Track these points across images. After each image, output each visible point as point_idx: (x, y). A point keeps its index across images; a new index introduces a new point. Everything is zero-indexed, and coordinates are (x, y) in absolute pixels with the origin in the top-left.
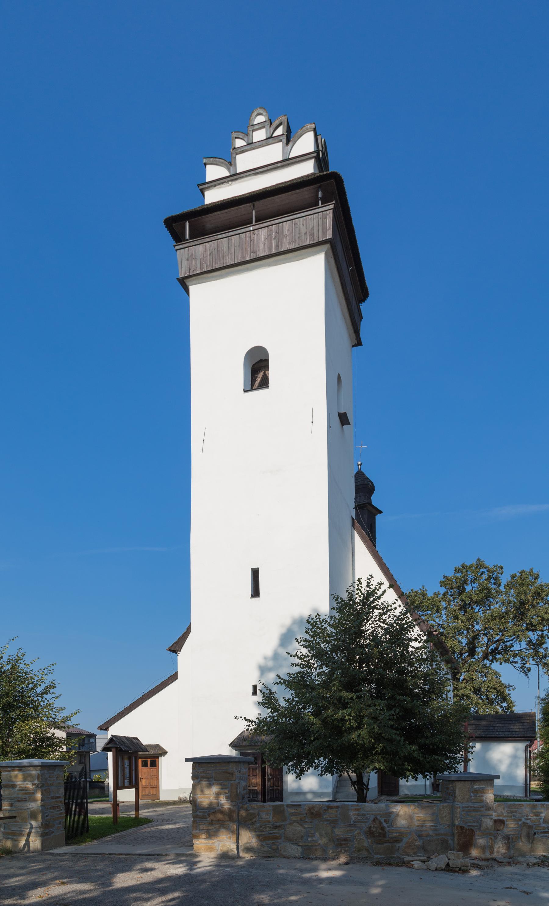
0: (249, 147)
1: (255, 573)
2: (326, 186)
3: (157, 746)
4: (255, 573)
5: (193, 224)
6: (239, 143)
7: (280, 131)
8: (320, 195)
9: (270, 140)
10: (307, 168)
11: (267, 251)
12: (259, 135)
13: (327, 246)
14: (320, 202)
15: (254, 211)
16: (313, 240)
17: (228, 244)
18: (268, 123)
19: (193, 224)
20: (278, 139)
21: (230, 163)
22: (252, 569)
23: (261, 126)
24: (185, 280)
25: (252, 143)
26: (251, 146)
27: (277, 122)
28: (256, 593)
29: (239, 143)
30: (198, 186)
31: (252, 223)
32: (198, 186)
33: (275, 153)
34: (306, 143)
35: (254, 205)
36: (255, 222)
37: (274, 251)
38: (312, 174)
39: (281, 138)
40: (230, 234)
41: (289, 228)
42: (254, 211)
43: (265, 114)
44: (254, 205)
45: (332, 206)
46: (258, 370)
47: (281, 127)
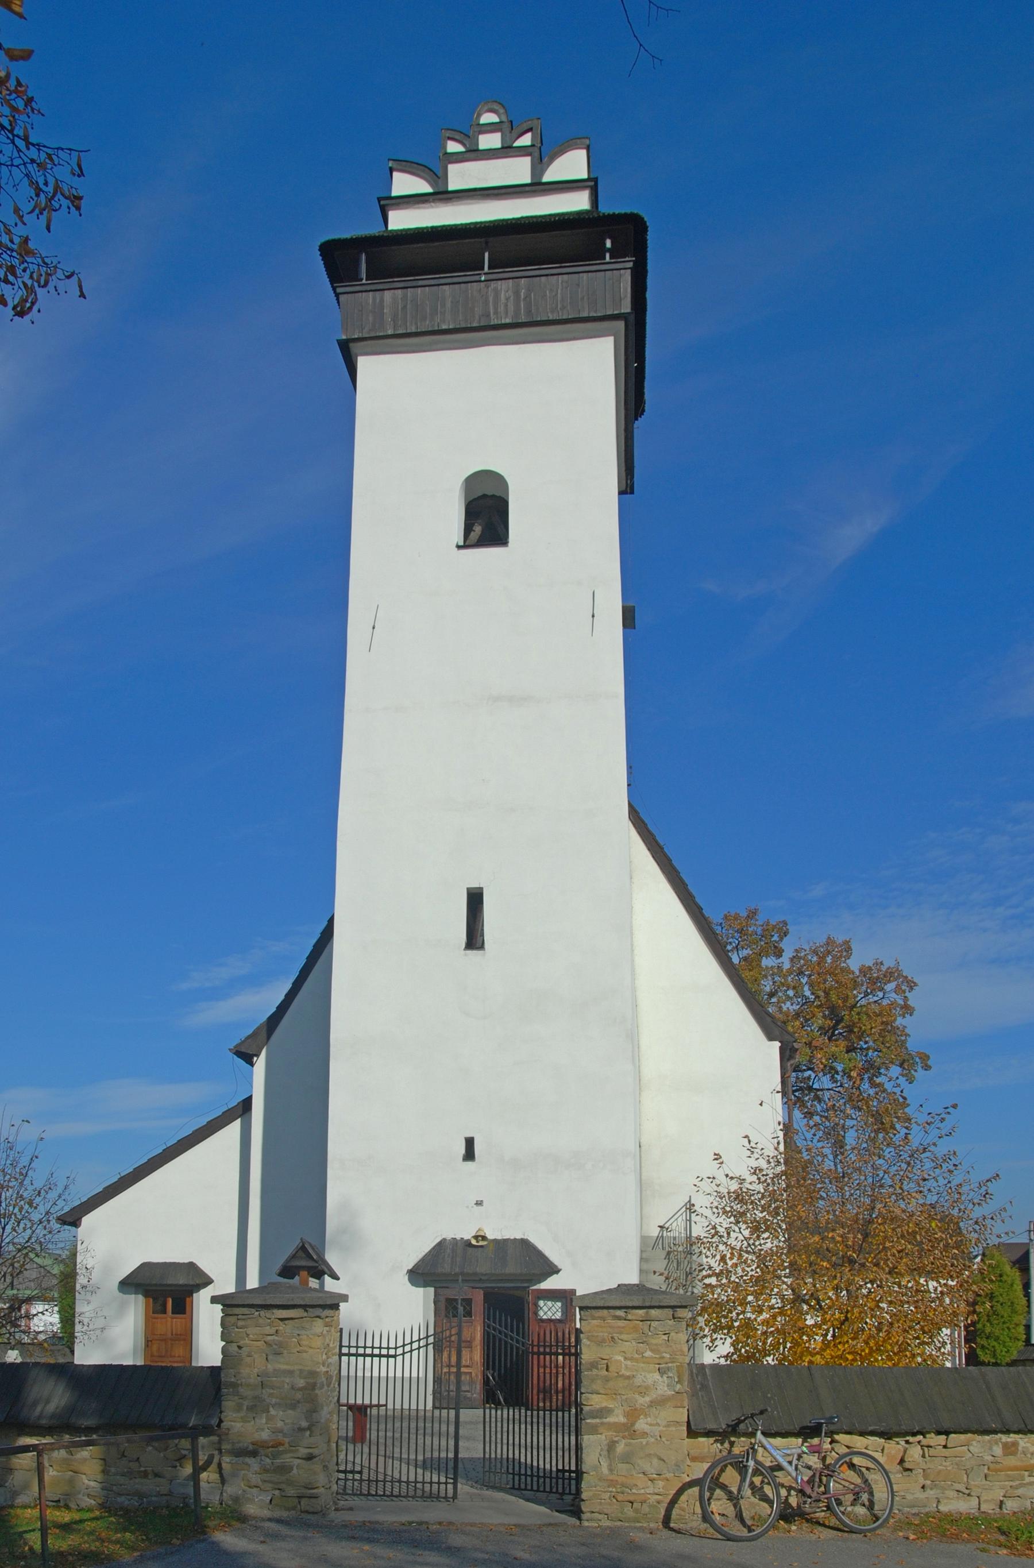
0: (468, 155)
1: (475, 900)
2: (607, 237)
3: (192, 1266)
4: (475, 900)
5: (364, 260)
6: (453, 147)
7: (526, 140)
8: (608, 244)
9: (507, 150)
10: (579, 202)
11: (511, 312)
12: (490, 141)
13: (621, 325)
14: (608, 255)
15: (487, 255)
16: (596, 312)
17: (444, 297)
18: (507, 126)
19: (364, 260)
20: (523, 151)
21: (436, 175)
22: (468, 889)
23: (491, 128)
24: (351, 345)
25: (477, 150)
26: (474, 153)
27: (525, 127)
28: (474, 939)
29: (453, 147)
30: (379, 199)
31: (483, 269)
32: (379, 199)
33: (518, 170)
34: (572, 164)
35: (487, 243)
36: (489, 268)
37: (523, 319)
38: (586, 212)
39: (531, 150)
40: (421, 283)
41: (557, 287)
42: (487, 255)
43: (502, 111)
44: (487, 243)
45: (631, 265)
46: (487, 516)
47: (529, 136)
